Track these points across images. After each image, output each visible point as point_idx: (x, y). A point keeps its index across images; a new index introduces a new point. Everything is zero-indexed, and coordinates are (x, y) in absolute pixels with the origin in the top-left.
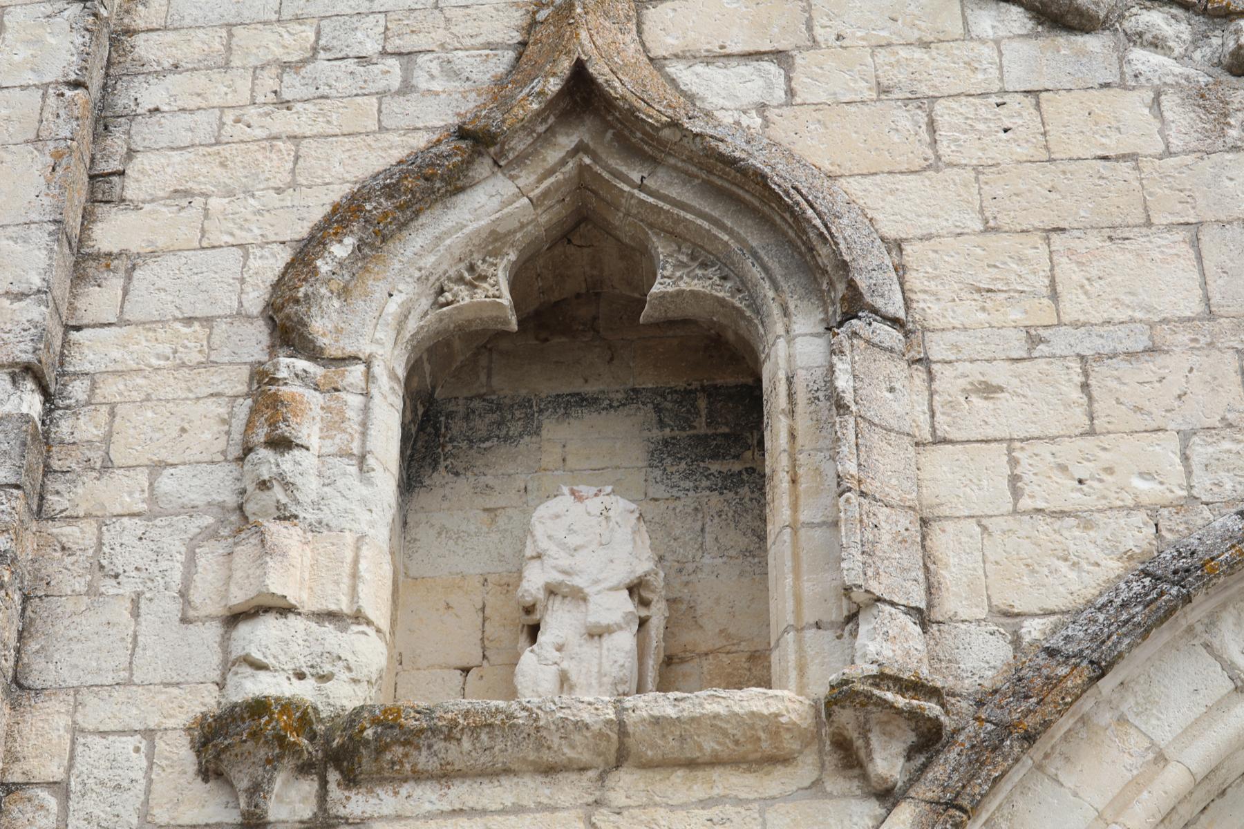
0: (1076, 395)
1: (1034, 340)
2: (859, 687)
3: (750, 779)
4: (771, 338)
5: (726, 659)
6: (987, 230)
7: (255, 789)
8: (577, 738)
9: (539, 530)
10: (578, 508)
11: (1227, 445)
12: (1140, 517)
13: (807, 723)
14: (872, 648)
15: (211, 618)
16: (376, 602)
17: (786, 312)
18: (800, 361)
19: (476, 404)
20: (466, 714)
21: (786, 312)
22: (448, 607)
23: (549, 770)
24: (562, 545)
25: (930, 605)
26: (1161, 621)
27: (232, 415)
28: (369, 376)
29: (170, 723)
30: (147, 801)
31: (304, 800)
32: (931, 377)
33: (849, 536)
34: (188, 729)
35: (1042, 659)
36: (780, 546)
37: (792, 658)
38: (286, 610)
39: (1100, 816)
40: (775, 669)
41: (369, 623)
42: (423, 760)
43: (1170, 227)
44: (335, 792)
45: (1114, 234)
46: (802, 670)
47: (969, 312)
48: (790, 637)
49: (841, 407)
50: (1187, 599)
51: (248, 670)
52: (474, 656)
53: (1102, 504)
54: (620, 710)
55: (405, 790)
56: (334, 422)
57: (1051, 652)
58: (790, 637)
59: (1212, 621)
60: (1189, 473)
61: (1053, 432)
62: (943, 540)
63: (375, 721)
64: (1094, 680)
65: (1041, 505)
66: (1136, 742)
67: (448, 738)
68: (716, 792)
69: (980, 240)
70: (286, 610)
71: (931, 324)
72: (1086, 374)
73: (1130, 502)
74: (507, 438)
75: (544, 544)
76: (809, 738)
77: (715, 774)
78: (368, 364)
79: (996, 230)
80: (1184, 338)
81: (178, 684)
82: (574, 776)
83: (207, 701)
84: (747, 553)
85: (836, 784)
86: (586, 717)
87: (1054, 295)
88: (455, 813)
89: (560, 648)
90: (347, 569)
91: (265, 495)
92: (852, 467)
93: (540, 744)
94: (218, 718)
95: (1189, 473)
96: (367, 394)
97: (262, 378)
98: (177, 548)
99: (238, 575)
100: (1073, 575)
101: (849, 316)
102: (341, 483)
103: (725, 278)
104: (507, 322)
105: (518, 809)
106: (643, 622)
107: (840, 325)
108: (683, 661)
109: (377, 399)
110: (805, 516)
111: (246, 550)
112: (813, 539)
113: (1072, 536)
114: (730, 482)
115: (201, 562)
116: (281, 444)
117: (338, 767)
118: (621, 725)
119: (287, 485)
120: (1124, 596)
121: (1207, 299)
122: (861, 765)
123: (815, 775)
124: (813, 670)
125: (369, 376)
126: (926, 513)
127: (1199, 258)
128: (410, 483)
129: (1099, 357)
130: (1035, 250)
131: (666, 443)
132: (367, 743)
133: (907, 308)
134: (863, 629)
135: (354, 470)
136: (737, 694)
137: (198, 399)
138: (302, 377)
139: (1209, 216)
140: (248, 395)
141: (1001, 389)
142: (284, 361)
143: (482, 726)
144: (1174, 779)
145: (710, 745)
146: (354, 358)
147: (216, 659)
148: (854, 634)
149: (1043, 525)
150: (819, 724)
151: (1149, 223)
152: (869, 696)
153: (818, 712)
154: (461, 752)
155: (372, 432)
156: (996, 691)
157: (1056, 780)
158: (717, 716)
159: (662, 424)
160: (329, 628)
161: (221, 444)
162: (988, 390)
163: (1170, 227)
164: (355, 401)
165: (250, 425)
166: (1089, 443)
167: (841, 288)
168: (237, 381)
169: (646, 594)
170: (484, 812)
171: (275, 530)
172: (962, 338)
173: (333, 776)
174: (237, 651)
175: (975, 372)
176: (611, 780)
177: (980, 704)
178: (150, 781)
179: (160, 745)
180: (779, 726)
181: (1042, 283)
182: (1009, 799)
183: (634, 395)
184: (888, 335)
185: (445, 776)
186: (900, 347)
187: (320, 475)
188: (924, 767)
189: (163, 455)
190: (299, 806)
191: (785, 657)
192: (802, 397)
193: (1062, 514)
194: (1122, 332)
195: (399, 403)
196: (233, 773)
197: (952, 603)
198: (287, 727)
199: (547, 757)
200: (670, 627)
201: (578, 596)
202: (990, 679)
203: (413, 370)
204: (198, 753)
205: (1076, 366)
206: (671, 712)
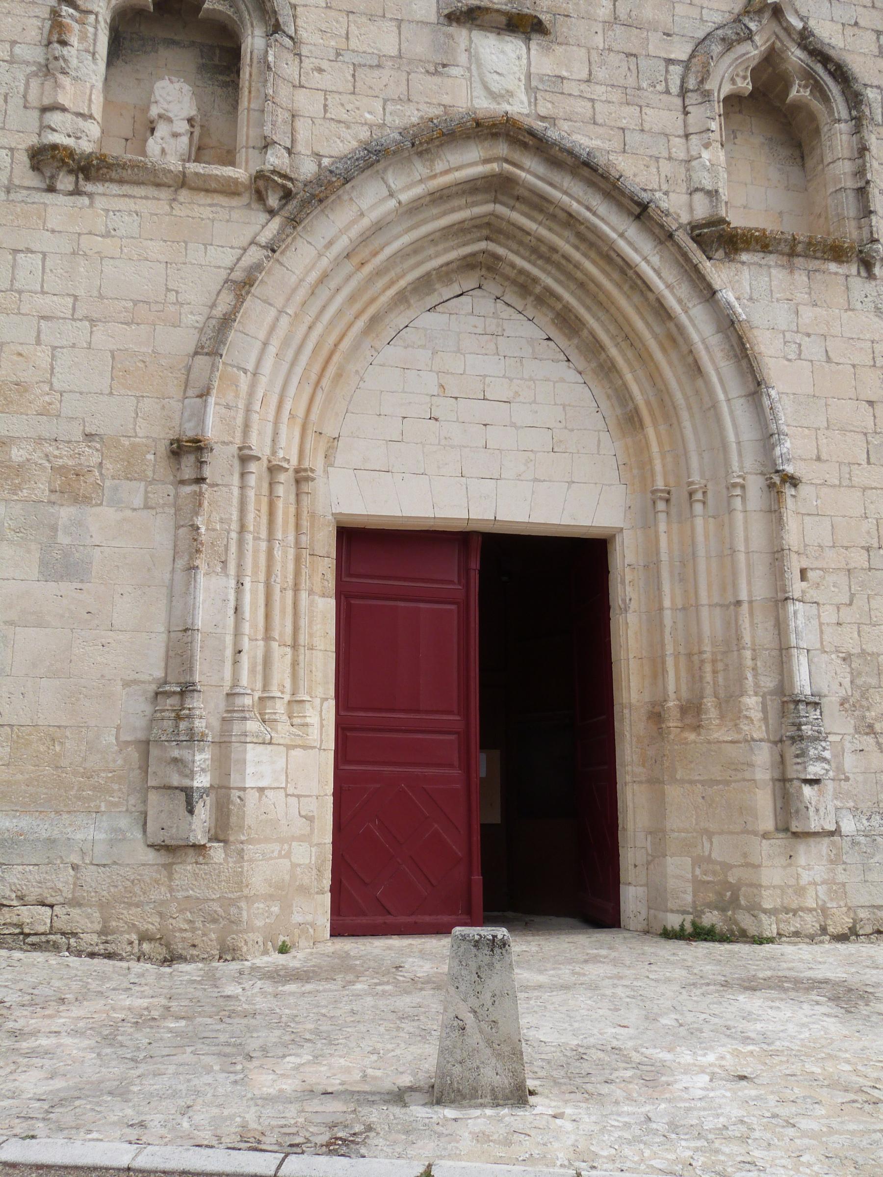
0: (350, 78)
1: (338, 54)
2: (268, 174)
3: (226, 199)
4: (246, 34)
5: (219, 151)
6: (327, 7)
7: (52, 177)
8: (168, 175)
9: (157, 93)
10: (171, 86)
11: (399, 107)
12: (366, 128)
13: (247, 182)
14: (272, 160)
15: (35, 108)
16: (97, 110)
17: (252, 26)
18: (256, 46)
19: (134, 36)
20: (130, 161)
21: (252, 26)
22: (121, 115)
23: (158, 185)
24: (165, 99)
25: (292, 147)
26: (368, 167)
27: (43, 26)
28: (97, 20)
29: (20, 147)
30: (11, 176)
31: (70, 183)
32: (301, 62)
33: (267, 117)
34: (27, 150)
35: (327, 173)
36: (242, 115)
37: (244, 158)
38: (64, 109)
39: (340, 231)
40: (238, 160)
41: (95, 119)
42: (113, 175)
43: (391, 19)
44: (81, 182)
45: (371, 18)
46: (247, 162)
47: (316, 38)
48: (244, 150)
49: (269, 68)
50: (378, 161)
51: (50, 131)
52: (130, 135)
53: (354, 121)
54: (184, 168)
55: (106, 185)
56: (83, 38)
57: (331, 172)
58: (244, 150)
59: (385, 170)
60: (384, 115)
61: (341, 90)
62: (299, 124)
63: (97, 158)
64: (344, 184)
65: (333, 117)
66: (355, 208)
67: (123, 168)
68: (215, 202)
69: (324, 10)
70: (64, 109)
71: (303, 41)
72: (354, 71)
73: (363, 122)
74: (145, 52)
75: (158, 98)
76: (248, 188)
77: (215, 195)
78: (97, 15)
79: (330, 8)
80: (390, 63)
81: (22, 132)
82: (166, 189)
83: (33, 140)
84: (229, 113)
85: (255, 205)
86: (172, 168)
87: (347, 38)
88: (124, 196)
89: (162, 139)
90: (87, 97)
91: (56, 63)
92: (271, 92)
93: (156, 176)
94: (39, 149)
95: (384, 115)
96: (96, 28)
97: (55, 14)
98: (21, 77)
99: (46, 93)
100: (341, 145)
101: (275, 32)
102: (85, 62)
103: (231, 6)
104: (149, 7)
105: (146, 198)
106: (192, 133)
107: (271, 35)
108: (204, 149)
109: (100, 31)
110: (252, 106)
111: (49, 84)
112: (255, 115)
113: (343, 131)
114: (225, 85)
115: (32, 85)
116: (63, 43)
117: (83, 173)
118: (184, 173)
119: (65, 60)
120: (357, 156)
121: (400, 50)
122: (264, 200)
123: (248, 201)
124: (251, 163)
125: (97, 20)
126: (294, 113)
127: (400, 34)
128: (109, 64)
129: (360, 65)
130: (343, 19)
131: (203, 65)
132: (93, 165)
133: (296, 33)
134: (269, 152)
135: (90, 58)
136: (225, 168)
137: (29, 17)
138: (71, 16)
139: (405, 18)
140: (49, 19)
141: (325, 71)
142: (64, 8)
143: (135, 166)
144: (366, 222)
145: (214, 185)
146: (91, 12)
147: (37, 124)
148: (266, 153)
149: (333, 125)
150: (251, 183)
151: (384, 16)
152: (269, 177)
153: (251, 179)
154: (127, 174)
155: (98, 44)
156: (311, 182)
157: (327, 216)
158: (217, 175)
159: (202, 57)
160: (80, 119)
161: (39, 38)
162: (320, 70)
163: (391, 19)
164: (91, 30)
165: (50, 32)
166: (352, 97)
167: (273, 21)
168: (45, 13)
169: (193, 123)
170: (134, 197)
171: (61, 77)
172: (313, 48)
173: (81, 176)
174: (45, 123)
175: (317, 62)
176: (179, 192)
177: (305, 185)
178: (12, 168)
179: (16, 155)
180: (238, 182)
181: (344, 32)
182: (311, 220)
183: (193, 44)
184: (288, 42)
185: (121, 182)
186: (291, 48)
187: (78, 58)
188: (285, 205)
189: (15, 38)
190: (68, 186)
191: (241, 156)
192: (255, 61)
193: (340, 122)
194: (369, 57)
195: (107, 33)
196: (44, 170)
197: (300, 147)
198: (65, 156)
199: (158, 181)
200: (200, 138)
201: (170, 120)
202: (309, 176)
203: (113, 19)
204: (31, 160)
205: (351, 67)
206: (202, 171)
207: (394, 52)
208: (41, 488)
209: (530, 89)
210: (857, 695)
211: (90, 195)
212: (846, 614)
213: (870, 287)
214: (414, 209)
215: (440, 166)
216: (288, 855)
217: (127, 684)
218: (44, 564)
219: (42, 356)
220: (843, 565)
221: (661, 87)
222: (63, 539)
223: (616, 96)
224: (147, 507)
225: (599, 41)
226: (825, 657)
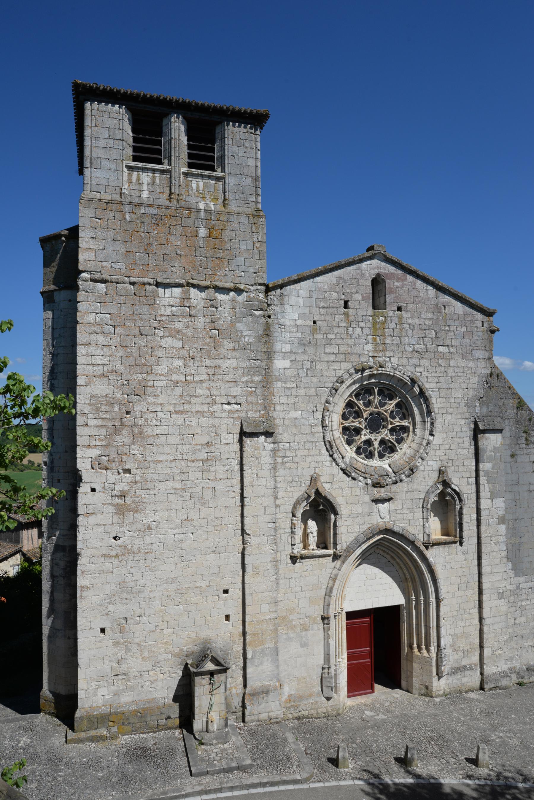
207: (361, 512)
208: (298, 629)
209: (390, 514)
211: (302, 563)
212: (452, 626)
213: (461, 548)
217: (317, 666)
218: (301, 644)
219: (297, 602)
221: (418, 507)
222: (304, 639)
223: (408, 511)
224: (318, 629)
225: (404, 498)
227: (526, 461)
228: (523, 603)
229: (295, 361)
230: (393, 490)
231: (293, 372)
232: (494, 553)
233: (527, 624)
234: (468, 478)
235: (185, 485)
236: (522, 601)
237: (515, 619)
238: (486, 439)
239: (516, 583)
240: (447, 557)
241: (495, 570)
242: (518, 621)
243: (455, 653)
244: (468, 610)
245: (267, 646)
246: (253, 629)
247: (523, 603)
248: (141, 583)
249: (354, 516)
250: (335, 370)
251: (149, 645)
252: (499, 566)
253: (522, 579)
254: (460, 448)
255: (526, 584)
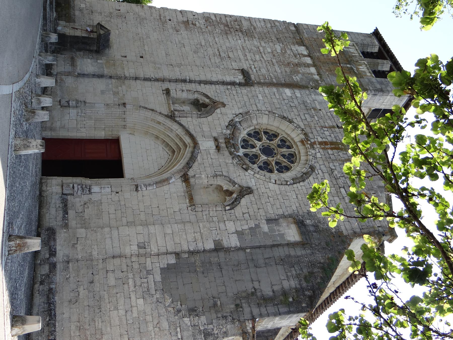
210: (93, 201)
214: (177, 135)
215: (184, 136)
216: (58, 120)
218: (103, 90)
220: (120, 200)
222: (107, 92)
225: (221, 160)
226: (100, 196)
227: (281, 276)
228: (131, 282)
229: (292, 99)
230: (225, 152)
231: (285, 97)
232: (184, 237)
233: (106, 288)
234: (248, 213)
235: (204, 46)
236: (133, 278)
237: (113, 271)
238: (288, 226)
239: (154, 269)
240: (175, 195)
241: (168, 238)
242: (110, 275)
243: (83, 204)
244: (125, 215)
245: (105, 70)
246: (117, 64)
247: (131, 282)
248: (146, 25)
249: (200, 126)
250: (296, 119)
251: (109, 24)
252: (173, 243)
253: (158, 278)
254: (272, 205)
255: (153, 284)
